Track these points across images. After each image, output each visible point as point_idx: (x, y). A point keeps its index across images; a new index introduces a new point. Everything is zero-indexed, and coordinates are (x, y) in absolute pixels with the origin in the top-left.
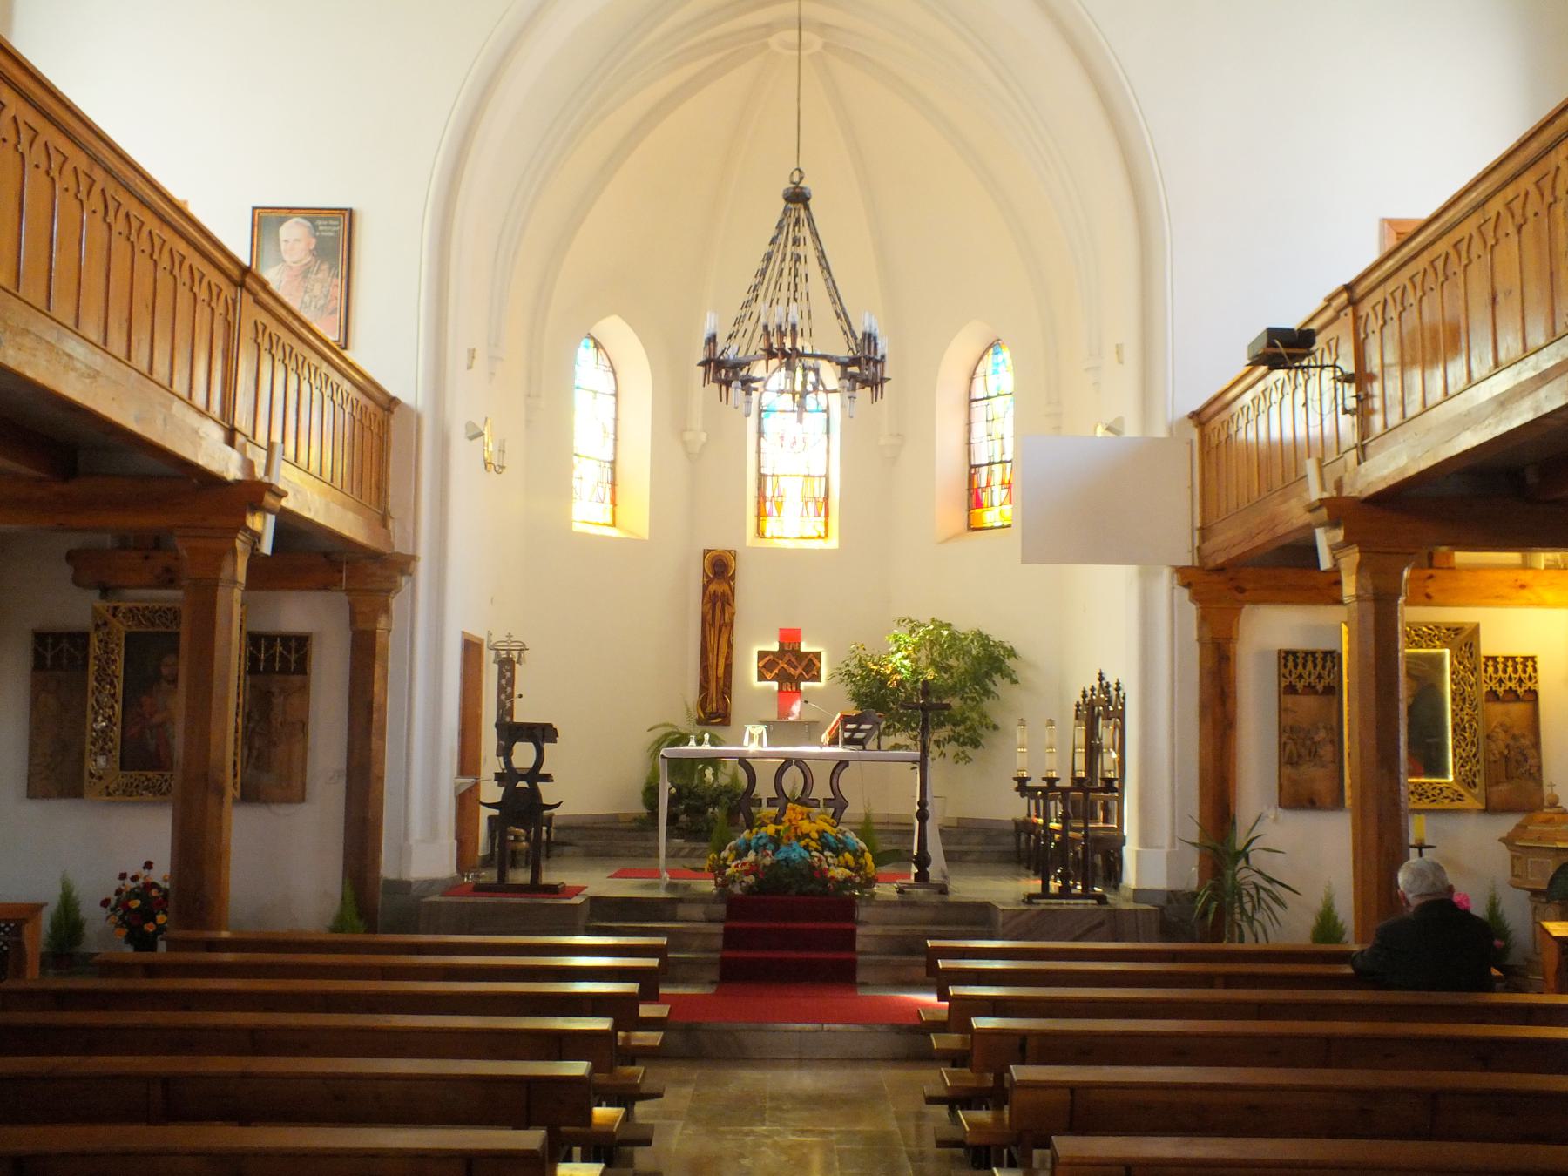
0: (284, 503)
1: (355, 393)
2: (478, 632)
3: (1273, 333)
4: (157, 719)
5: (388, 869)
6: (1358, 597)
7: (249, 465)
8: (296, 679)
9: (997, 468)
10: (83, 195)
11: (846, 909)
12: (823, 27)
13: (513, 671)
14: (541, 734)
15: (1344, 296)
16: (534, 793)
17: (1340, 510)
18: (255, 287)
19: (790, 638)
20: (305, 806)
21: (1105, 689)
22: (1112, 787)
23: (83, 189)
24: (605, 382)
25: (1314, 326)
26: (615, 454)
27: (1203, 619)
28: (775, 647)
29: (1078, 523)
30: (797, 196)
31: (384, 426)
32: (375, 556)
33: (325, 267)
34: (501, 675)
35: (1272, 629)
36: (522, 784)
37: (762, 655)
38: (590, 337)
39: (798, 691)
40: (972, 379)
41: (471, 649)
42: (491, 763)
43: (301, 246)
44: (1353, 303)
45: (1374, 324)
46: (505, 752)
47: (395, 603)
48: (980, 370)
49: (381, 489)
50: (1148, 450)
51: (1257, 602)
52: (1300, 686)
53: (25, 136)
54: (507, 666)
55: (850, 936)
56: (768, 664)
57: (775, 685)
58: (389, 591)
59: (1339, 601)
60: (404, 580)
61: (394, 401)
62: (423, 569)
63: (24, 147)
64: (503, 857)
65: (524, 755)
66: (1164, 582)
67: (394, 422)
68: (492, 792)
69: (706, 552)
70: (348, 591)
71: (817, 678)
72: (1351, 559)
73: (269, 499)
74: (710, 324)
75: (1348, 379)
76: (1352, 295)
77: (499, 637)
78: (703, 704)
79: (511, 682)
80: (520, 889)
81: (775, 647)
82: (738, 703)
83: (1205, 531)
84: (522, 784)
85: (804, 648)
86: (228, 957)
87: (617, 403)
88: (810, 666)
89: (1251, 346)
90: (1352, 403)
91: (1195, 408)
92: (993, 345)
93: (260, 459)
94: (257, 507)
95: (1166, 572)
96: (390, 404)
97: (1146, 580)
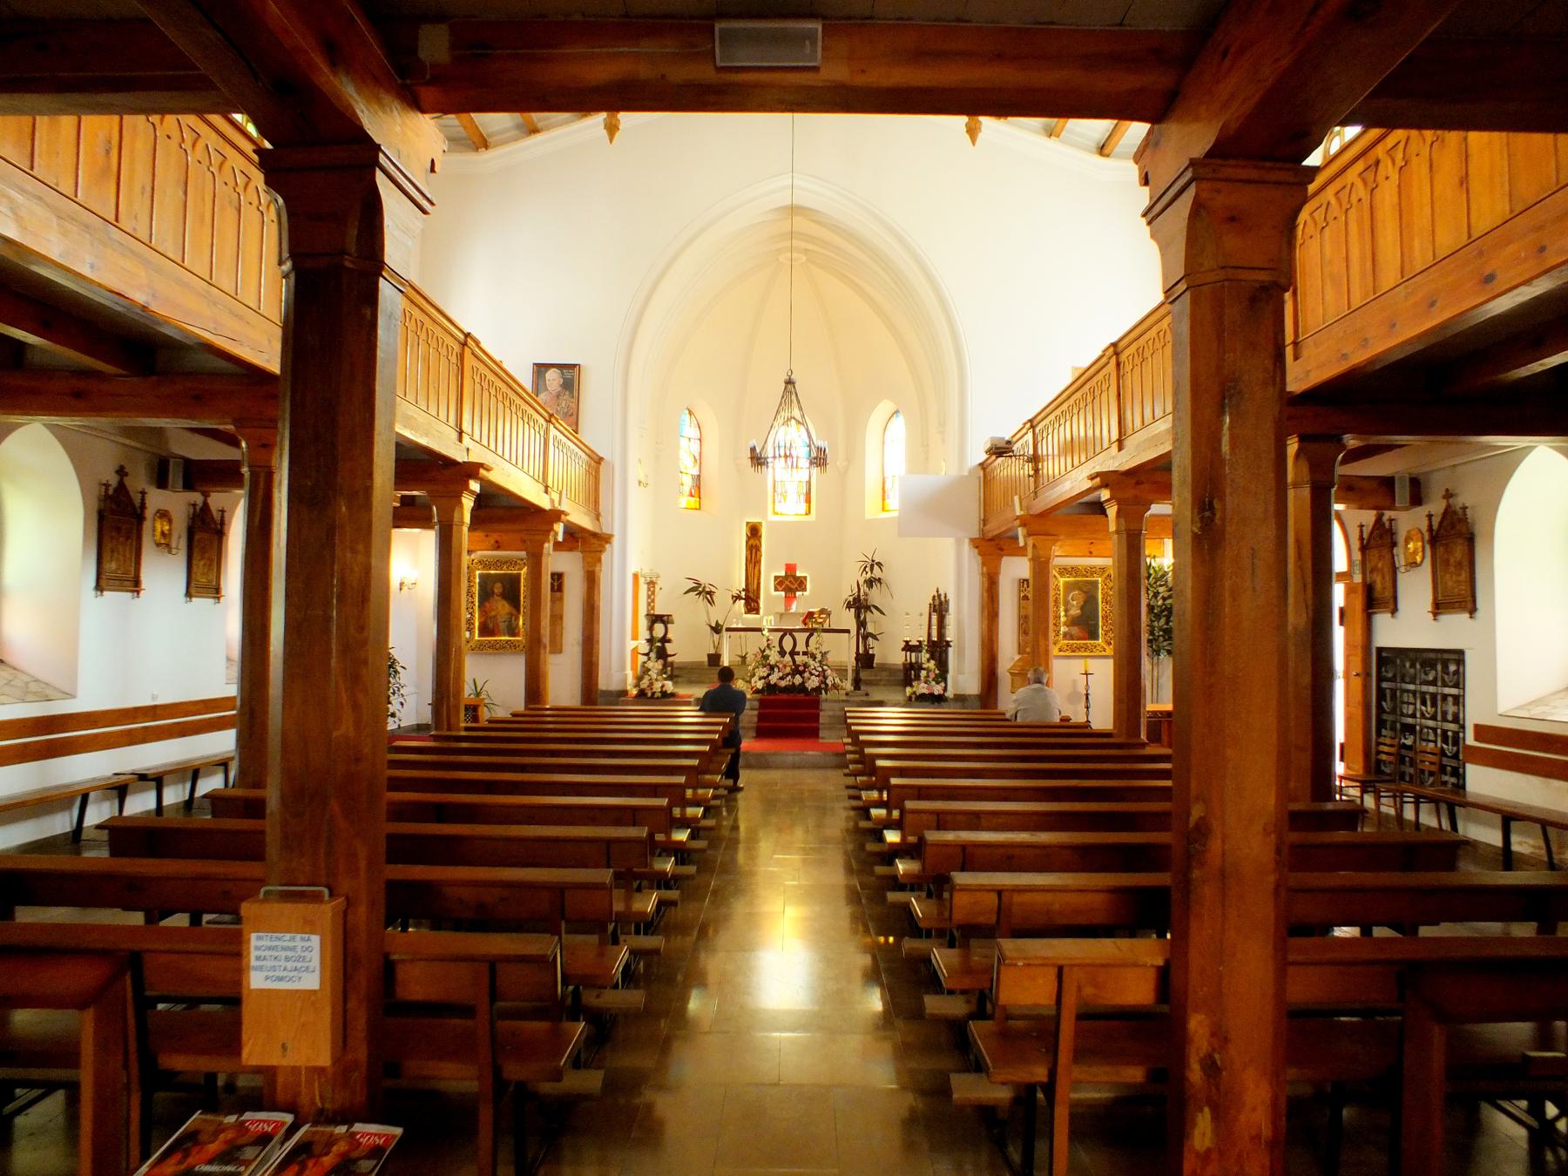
6: (1117, 532)
7: (552, 501)
11: (816, 704)
19: (790, 568)
22: (948, 644)
24: (694, 433)
27: (984, 564)
28: (783, 573)
29: (929, 511)
30: (789, 382)
31: (597, 471)
32: (594, 535)
41: (636, 576)
44: (1033, 427)
45: (1128, 368)
46: (651, 629)
47: (604, 557)
49: (596, 502)
50: (961, 481)
54: (651, 584)
55: (817, 716)
56: (780, 583)
62: (616, 541)
63: (188, 145)
65: (659, 630)
66: (966, 546)
73: (482, 471)
74: (751, 444)
76: (1032, 424)
77: (646, 571)
81: (783, 573)
83: (985, 521)
85: (798, 574)
86: (464, 745)
88: (801, 584)
91: (1114, 340)
93: (555, 496)
94: (475, 476)
96: (599, 460)
97: (959, 543)
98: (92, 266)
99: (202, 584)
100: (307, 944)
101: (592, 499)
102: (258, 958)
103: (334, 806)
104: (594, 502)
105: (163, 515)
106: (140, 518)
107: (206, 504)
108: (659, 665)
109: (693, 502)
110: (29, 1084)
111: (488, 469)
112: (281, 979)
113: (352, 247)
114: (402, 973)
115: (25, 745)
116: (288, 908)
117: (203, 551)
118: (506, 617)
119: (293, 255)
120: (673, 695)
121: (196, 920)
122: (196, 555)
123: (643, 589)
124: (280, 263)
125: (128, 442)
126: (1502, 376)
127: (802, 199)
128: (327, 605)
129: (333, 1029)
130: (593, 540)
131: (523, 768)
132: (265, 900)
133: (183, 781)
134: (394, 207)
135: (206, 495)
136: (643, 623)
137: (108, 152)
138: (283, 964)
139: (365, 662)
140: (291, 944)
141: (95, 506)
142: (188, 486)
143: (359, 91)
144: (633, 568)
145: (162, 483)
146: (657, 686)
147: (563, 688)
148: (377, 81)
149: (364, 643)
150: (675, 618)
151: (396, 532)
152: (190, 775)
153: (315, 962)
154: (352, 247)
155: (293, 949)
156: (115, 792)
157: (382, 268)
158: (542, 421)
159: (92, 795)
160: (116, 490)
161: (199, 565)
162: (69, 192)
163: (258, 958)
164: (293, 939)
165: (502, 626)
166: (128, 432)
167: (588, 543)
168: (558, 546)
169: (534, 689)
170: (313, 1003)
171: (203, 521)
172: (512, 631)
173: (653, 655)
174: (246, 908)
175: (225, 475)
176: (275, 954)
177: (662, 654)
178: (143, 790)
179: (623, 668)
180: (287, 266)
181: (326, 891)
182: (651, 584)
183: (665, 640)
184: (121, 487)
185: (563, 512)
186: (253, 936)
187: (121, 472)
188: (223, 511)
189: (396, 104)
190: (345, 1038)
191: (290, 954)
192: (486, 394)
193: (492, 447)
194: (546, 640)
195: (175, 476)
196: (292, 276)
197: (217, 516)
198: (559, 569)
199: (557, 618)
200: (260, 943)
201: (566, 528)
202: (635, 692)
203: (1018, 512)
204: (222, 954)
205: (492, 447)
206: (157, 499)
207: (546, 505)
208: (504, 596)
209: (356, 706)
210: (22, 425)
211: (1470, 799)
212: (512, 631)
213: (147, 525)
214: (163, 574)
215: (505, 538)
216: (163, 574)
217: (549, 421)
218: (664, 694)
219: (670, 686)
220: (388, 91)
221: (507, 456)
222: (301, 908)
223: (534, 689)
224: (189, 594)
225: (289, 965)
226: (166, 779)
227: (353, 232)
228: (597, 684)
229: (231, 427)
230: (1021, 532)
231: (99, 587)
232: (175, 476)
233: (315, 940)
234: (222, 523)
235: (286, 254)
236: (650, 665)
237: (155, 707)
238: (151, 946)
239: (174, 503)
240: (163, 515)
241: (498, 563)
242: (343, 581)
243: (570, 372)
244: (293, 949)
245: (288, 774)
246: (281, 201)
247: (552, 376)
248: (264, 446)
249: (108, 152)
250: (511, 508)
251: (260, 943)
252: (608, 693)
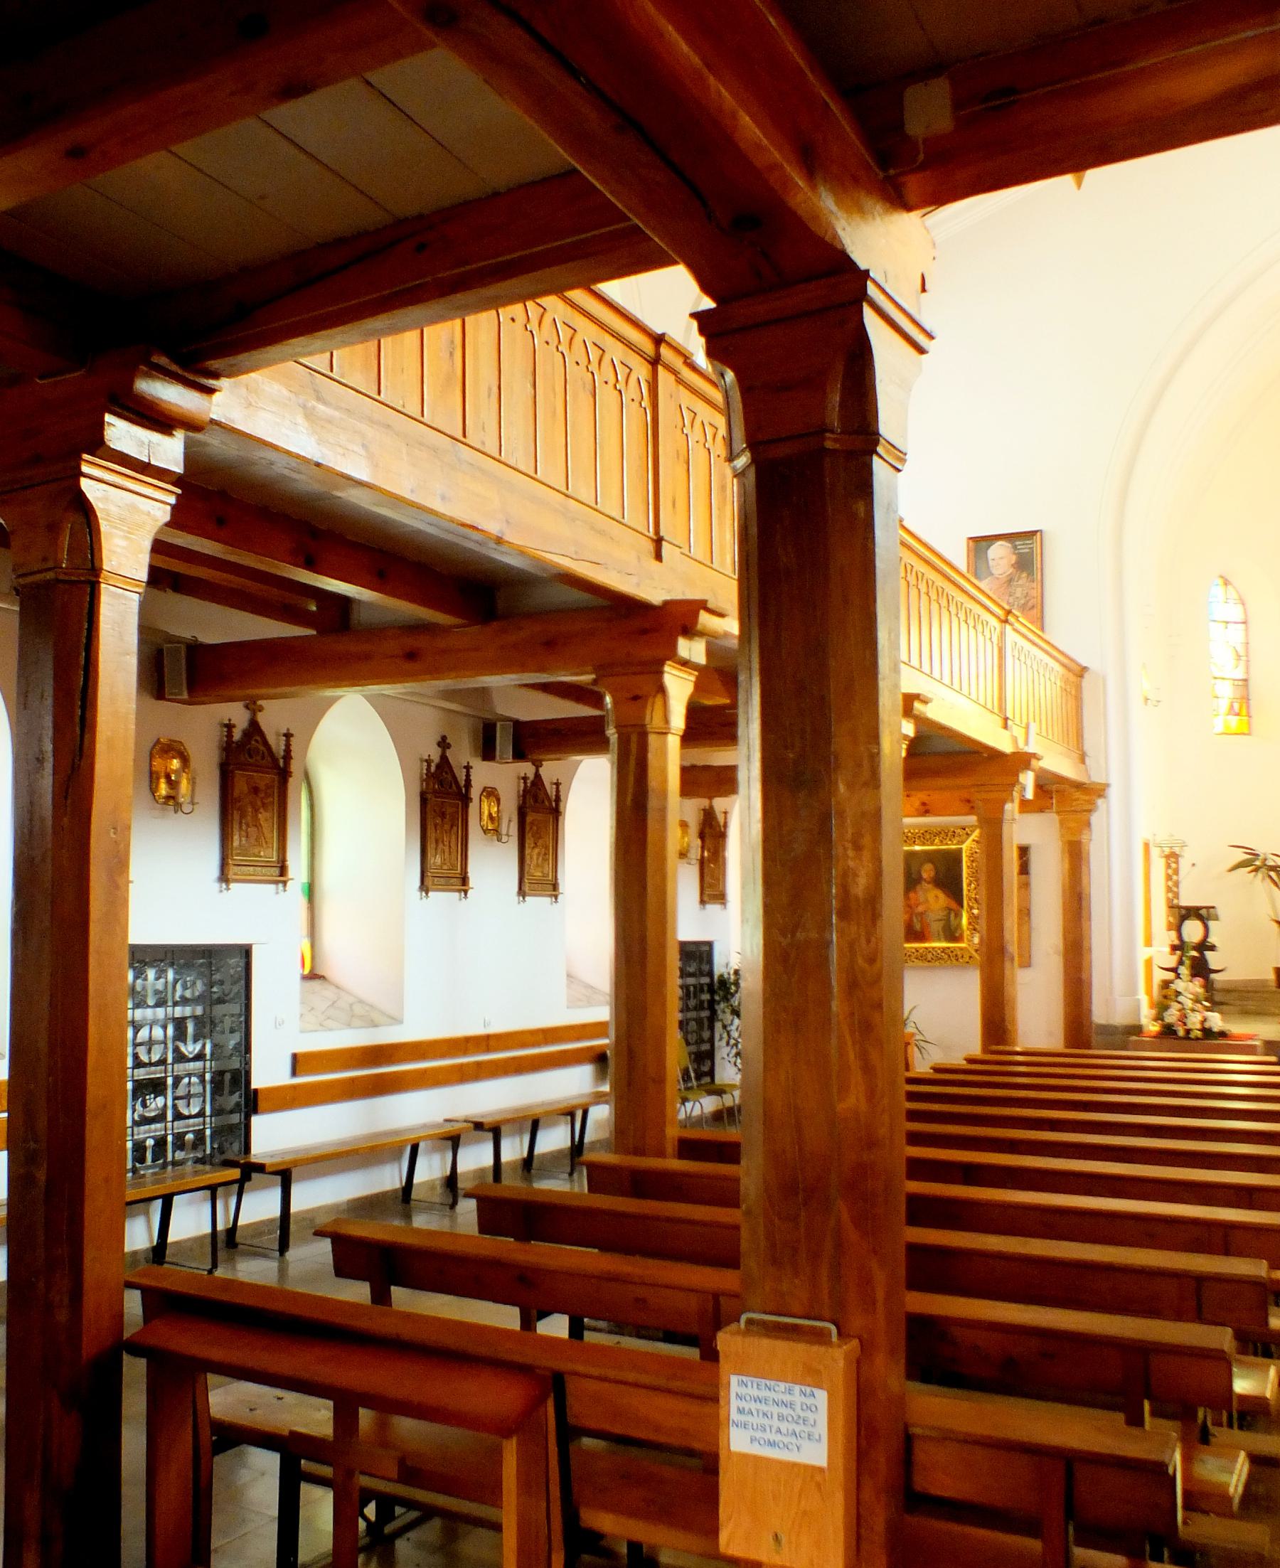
4: (920, 909)
7: (1015, 740)
10: (533, 325)
13: (1177, 862)
23: (709, 437)
26: (1247, 672)
31: (1079, 688)
32: (1079, 786)
33: (1024, 575)
41: (1147, 846)
43: (1005, 561)
47: (1095, 819)
53: (564, 333)
54: (1172, 858)
58: (1090, 811)
59: (134, 1081)
60: (1100, 802)
61: (1085, 669)
62: (1114, 793)
63: (533, 325)
65: (1193, 931)
67: (1086, 682)
70: (1058, 813)
87: (1247, 630)
93: (1019, 732)
94: (689, 631)
96: (1081, 672)
98: (443, 498)
99: (537, 878)
100: (809, 1401)
102: (741, 1411)
103: (842, 1210)
104: (1075, 739)
105: (490, 793)
106: (466, 799)
107: (537, 775)
108: (1196, 986)
109: (1235, 723)
110: (410, 1504)
111: (925, 702)
112: (772, 1444)
113: (834, 418)
114: (922, 1454)
115: (353, 1080)
116: (782, 1346)
117: (538, 836)
118: (942, 914)
119: (754, 444)
120: (1223, 1034)
121: (576, 1330)
122: (529, 842)
123: (1159, 866)
124: (731, 458)
125: (453, 706)
126: (827, 202)
128: (825, 925)
129: (847, 1529)
130: (1077, 795)
132: (747, 1333)
133: (521, 1132)
134: (885, 348)
135: (538, 765)
136: (1161, 916)
137: (451, 354)
138: (776, 1423)
139: (879, 1006)
140: (787, 1398)
141: (417, 790)
142: (519, 755)
143: (838, 203)
144: (1142, 833)
145: (488, 752)
146: (1194, 1021)
147: (1038, 1023)
148: (856, 180)
149: (878, 978)
150: (1221, 911)
152: (529, 1124)
153: (822, 1428)
154: (834, 418)
155: (791, 1405)
156: (449, 1143)
157: (877, 443)
158: (994, 622)
159: (422, 1146)
160: (438, 766)
161: (533, 854)
162: (414, 410)
163: (741, 1411)
164: (790, 1392)
165: (936, 927)
166: (449, 695)
167: (1068, 799)
168: (1025, 806)
169: (996, 1023)
170: (818, 1485)
171: (536, 798)
172: (952, 934)
173: (1184, 971)
174: (726, 1341)
175: (584, 737)
176: (764, 1407)
177: (1200, 969)
178: (478, 1141)
179: (1133, 991)
180: (742, 461)
181: (833, 1328)
182: (1172, 858)
183: (1204, 946)
184: (444, 762)
185: (1034, 755)
186: (734, 1380)
187: (443, 743)
188: (558, 784)
189: (879, 207)
190: (859, 1538)
191: (785, 1411)
192: (914, 592)
193: (926, 668)
194: (1013, 948)
195: (504, 743)
196: (751, 475)
197: (551, 791)
198: (1024, 842)
199: (1025, 913)
200: (742, 1391)
201: (1037, 778)
202: (1154, 1028)
204: (669, 1391)
205: (926, 668)
206: (484, 774)
207: (1006, 747)
208: (939, 882)
209: (868, 1069)
210: (340, 697)
212: (952, 934)
213: (473, 808)
214: (493, 865)
215: (936, 798)
216: (493, 865)
217: (1006, 621)
218: (1208, 1033)
219: (1216, 1021)
220: (869, 192)
221: (947, 680)
222: (800, 1349)
223: (996, 1023)
224: (522, 893)
225: (784, 1427)
226: (504, 1129)
227: (835, 398)
229: (586, 678)
231: (424, 888)
232: (504, 743)
233: (822, 1397)
234: (558, 799)
235: (740, 444)
236: (1179, 985)
237: (488, 1037)
238: (580, 1368)
239: (499, 778)
240: (490, 793)
241: (926, 835)
242: (845, 889)
243: (1026, 547)
244: (791, 1405)
245: (775, 1158)
246: (730, 375)
247: (999, 554)
248: (636, 698)
249: (451, 354)
250: (949, 754)
251: (742, 1391)
252: (1108, 1030)
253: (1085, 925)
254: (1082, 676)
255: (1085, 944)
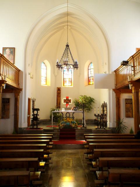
0: (7, 83)
1: (15, 69)
2: (30, 98)
3: (124, 62)
5: (19, 126)
7: (2, 78)
8: (8, 104)
9: (92, 77)
12: (70, 26)
14: (38, 110)
15: (132, 57)
16: (37, 117)
17: (132, 82)
18: (3, 57)
19: (67, 98)
20: (9, 119)
21: (105, 103)
22: (106, 115)
25: (128, 61)
27: (116, 95)
28: (65, 99)
30: (67, 46)
31: (19, 73)
34: (33, 103)
35: (125, 96)
36: (35, 116)
37: (64, 100)
38: (43, 62)
39: (68, 104)
40: (89, 67)
41: (29, 100)
42: (32, 113)
43: (8, 52)
44: (133, 58)
45: (135, 60)
46: (33, 112)
47: (20, 94)
48: (89, 66)
51: (122, 93)
52: (128, 103)
54: (33, 102)
56: (65, 101)
57: (66, 103)
60: (21, 92)
61: (20, 70)
62: (23, 90)
64: (33, 125)
65: (35, 112)
67: (20, 73)
68: (32, 117)
69: (57, 88)
70: (14, 93)
71: (71, 102)
72: (133, 88)
73: (5, 82)
75: (133, 67)
76: (133, 57)
78: (57, 106)
79: (34, 103)
80: (35, 129)
81: (65, 99)
82: (61, 106)
83: (116, 85)
84: (35, 116)
85: (69, 99)
88: (70, 101)
89: (121, 63)
90: (133, 70)
91: (132, 55)
92: (91, 63)
94: (3, 83)
95: (112, 89)
96: (19, 71)
97: (109, 90)
101: (17, 80)
127: (71, 11)
131: (16, 139)
151: (116, 127)
182: (33, 102)
183: (37, 115)
185: (5, 81)
203: (129, 80)
211: (115, 126)
221: (10, 78)
223: (77, 132)
228: (18, 126)
230: (130, 86)
253: (18, 111)
254: (19, 71)
255: (18, 114)
